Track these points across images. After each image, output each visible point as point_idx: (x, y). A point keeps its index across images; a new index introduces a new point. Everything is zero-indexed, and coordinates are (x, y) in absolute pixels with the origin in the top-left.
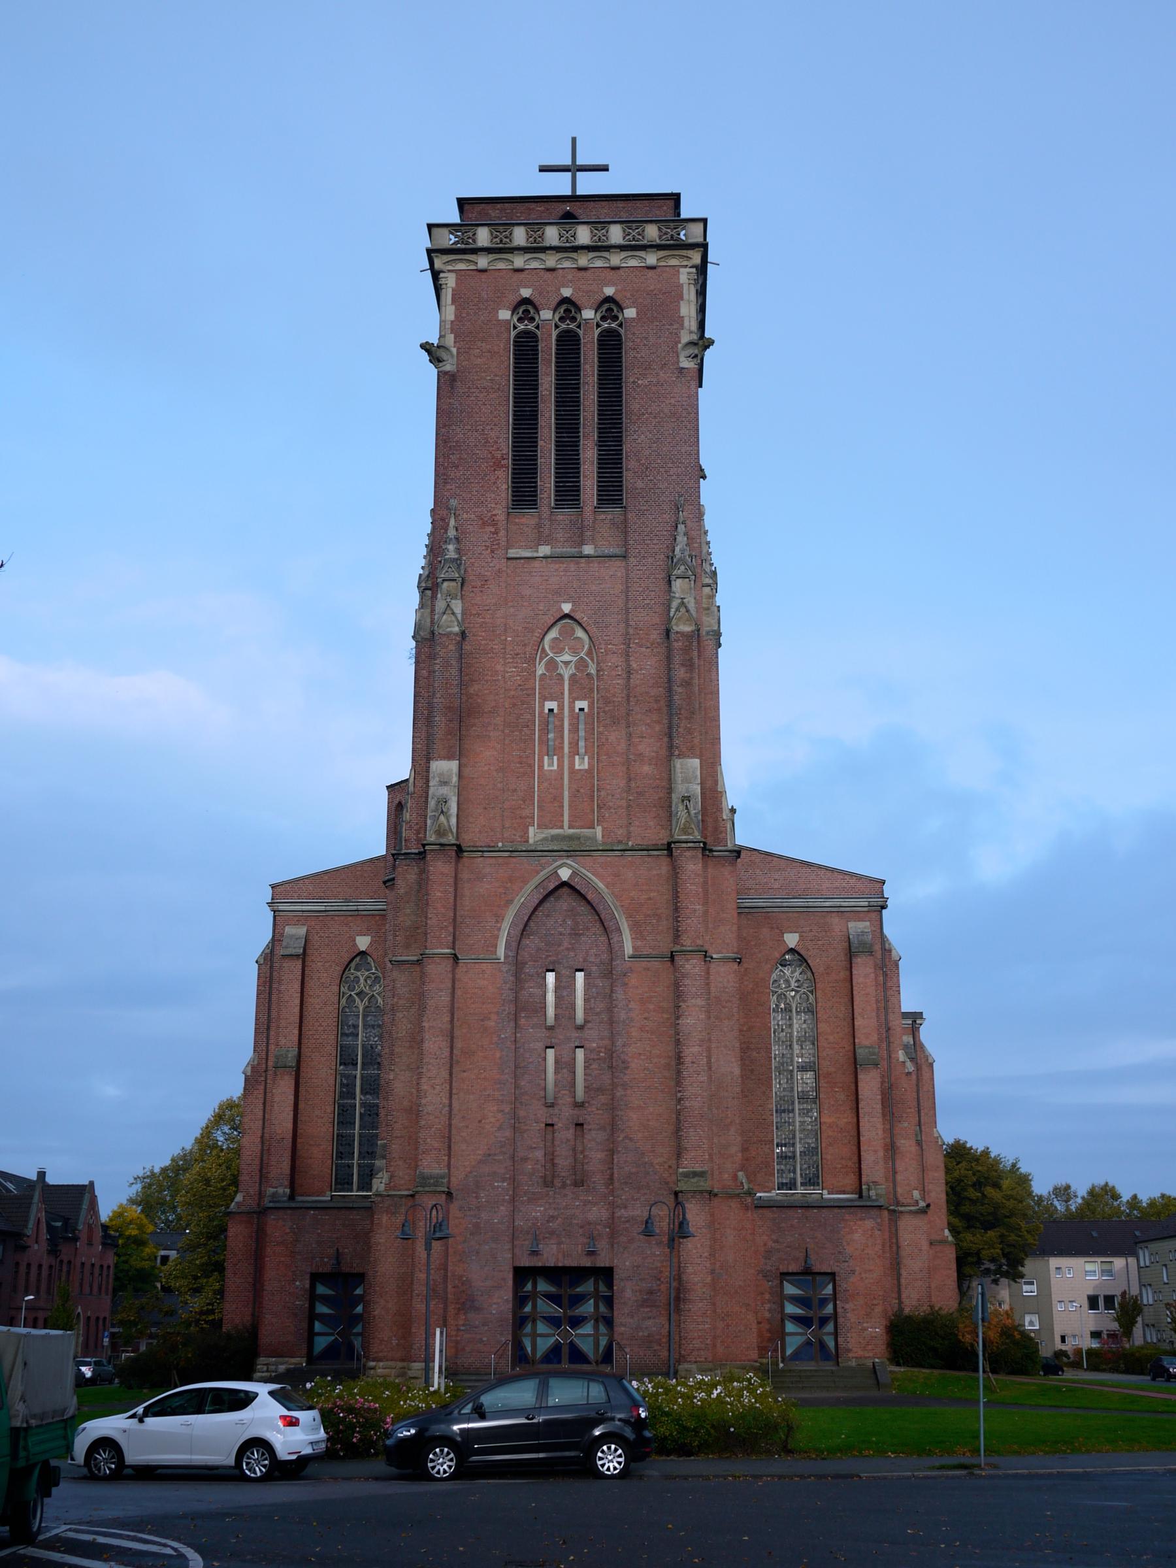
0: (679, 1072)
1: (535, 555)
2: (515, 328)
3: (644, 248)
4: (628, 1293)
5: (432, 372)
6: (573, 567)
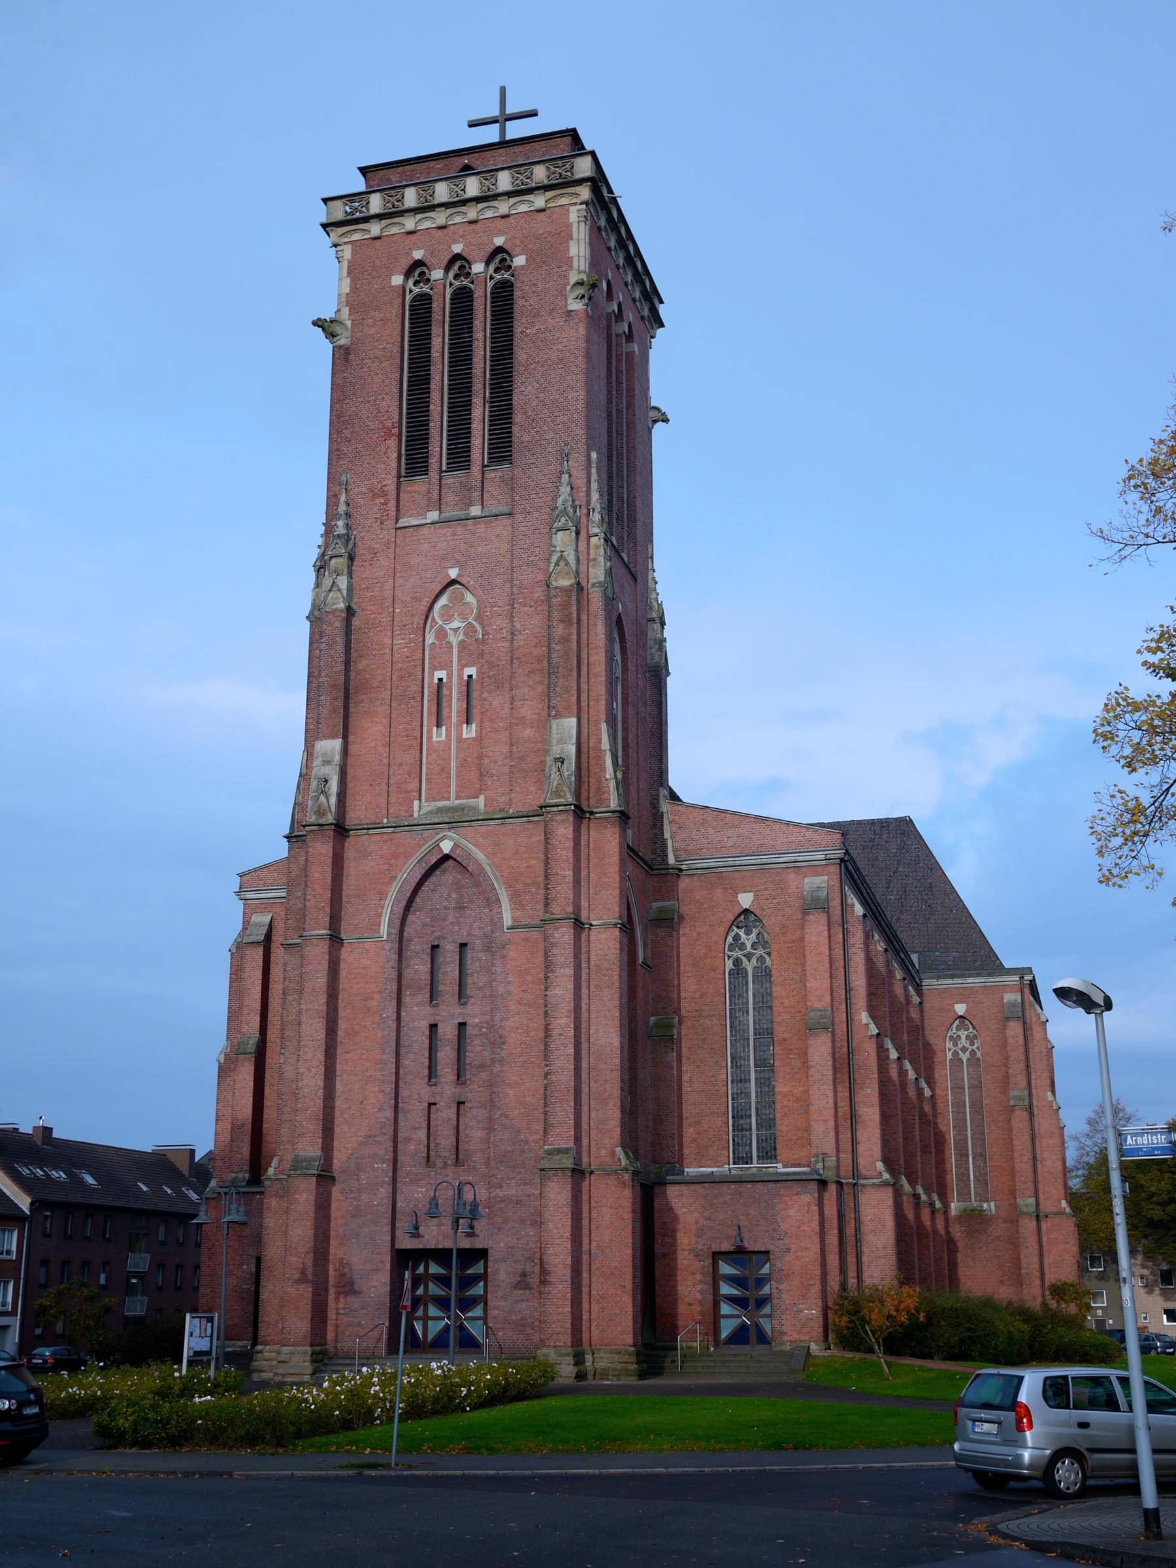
0: (546, 1045)
1: (424, 522)
2: (411, 291)
3: (531, 191)
4: (502, 1276)
5: (327, 347)
6: (460, 530)
